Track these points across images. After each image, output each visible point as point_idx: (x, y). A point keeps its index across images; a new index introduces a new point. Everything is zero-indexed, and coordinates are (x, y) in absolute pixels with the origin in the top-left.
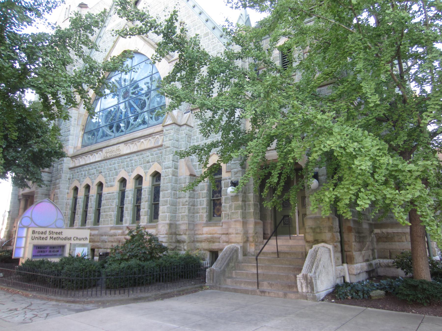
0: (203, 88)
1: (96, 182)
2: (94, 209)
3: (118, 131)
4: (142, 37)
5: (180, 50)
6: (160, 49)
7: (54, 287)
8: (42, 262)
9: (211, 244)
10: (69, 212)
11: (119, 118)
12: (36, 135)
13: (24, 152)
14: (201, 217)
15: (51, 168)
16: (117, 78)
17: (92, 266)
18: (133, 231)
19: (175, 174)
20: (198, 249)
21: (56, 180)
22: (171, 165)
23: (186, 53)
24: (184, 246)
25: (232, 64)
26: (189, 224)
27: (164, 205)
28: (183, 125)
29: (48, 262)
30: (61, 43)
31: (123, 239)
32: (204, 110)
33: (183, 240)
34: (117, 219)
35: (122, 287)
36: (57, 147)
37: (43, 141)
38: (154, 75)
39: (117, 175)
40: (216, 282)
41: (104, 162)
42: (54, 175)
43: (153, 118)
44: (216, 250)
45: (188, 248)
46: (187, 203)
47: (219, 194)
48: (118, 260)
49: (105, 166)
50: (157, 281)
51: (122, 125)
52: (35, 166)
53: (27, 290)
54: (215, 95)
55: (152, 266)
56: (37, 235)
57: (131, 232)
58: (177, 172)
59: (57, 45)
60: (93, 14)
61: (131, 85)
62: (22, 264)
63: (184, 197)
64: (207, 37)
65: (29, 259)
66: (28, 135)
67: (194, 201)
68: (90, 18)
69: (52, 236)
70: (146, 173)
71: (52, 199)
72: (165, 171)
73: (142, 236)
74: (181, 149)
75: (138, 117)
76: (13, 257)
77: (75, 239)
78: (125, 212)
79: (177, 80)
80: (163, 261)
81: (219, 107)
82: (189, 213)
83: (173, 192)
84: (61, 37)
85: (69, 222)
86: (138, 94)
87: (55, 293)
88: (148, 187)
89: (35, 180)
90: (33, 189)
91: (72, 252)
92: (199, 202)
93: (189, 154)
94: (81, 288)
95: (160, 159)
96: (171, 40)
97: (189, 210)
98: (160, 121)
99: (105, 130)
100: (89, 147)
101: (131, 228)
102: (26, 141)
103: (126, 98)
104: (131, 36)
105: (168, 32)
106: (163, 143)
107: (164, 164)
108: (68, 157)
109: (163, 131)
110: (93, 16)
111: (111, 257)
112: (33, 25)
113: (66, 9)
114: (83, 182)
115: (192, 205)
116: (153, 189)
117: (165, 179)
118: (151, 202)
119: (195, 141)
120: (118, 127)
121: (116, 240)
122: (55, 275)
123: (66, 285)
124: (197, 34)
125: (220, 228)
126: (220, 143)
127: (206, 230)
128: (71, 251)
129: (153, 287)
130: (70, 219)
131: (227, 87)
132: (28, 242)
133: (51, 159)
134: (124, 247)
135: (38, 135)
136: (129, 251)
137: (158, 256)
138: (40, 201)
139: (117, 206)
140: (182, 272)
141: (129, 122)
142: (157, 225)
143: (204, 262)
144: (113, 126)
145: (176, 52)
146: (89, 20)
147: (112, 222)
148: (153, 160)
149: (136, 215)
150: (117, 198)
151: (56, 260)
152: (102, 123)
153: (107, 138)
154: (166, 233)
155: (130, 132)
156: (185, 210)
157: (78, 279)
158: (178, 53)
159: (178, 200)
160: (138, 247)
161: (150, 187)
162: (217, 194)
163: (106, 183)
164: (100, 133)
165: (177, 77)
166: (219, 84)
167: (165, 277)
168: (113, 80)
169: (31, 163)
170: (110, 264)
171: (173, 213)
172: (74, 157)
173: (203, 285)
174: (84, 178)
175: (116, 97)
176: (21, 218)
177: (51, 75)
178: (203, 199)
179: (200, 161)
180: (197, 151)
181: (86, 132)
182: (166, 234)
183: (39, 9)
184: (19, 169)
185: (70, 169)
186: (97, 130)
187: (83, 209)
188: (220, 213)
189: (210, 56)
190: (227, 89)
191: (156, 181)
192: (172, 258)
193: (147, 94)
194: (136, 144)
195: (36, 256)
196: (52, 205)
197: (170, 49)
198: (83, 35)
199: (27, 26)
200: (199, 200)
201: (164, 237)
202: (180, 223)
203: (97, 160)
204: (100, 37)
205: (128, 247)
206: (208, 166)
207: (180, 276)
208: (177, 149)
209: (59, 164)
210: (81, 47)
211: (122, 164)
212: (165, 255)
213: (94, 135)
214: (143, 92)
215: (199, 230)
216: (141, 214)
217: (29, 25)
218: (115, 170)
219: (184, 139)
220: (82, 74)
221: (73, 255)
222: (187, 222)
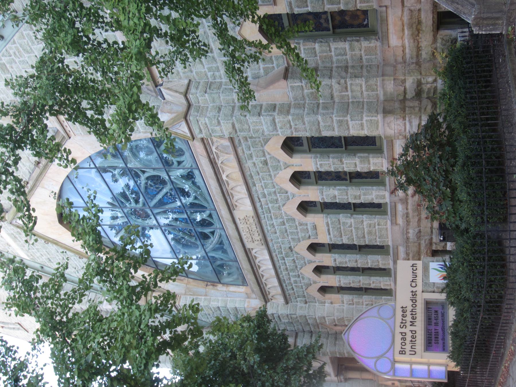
0: (109, 61)
1: (308, 256)
2: (358, 256)
3: (210, 224)
4: (30, 191)
5: (41, 114)
6: (47, 154)
7: (500, 311)
8: (455, 334)
9: (424, 29)
10: (366, 299)
11: (187, 222)
12: (231, 360)
13: (263, 376)
14: (369, 51)
15: (286, 333)
16: (112, 233)
17: (465, 250)
18: (399, 183)
19: (285, 109)
20: (433, 53)
21: (309, 324)
22: (269, 119)
23: (45, 99)
24: (427, 83)
25: (55, 7)
26: (383, 75)
27: (348, 126)
28: (187, 99)
29: (456, 324)
30: (63, 328)
31: (413, 200)
32: (154, 58)
33: (415, 85)
34: (376, 213)
35: (505, 194)
36: (250, 325)
37: (240, 349)
38: (97, 166)
39: (294, 220)
40: (501, 11)
41: (270, 245)
42: (300, 327)
43: (178, 159)
44: (436, 16)
45: (431, 75)
46: (342, 81)
47: (320, 18)
48: (453, 205)
49: (278, 243)
50: (494, 131)
51: (199, 218)
52: (286, 357)
53: (503, 354)
54: (119, 37)
55: (466, 140)
56: (408, 347)
57: (401, 186)
58: (282, 105)
59: (69, 334)
60: (3, 278)
61: (122, 206)
62: (456, 366)
63: (331, 87)
64: (8, 66)
65: (449, 357)
66: (232, 373)
67: (337, 67)
68: (11, 282)
69: (408, 324)
70: (287, 166)
71: (343, 327)
72: (281, 128)
73: (408, 165)
74: (236, 101)
75: (180, 189)
76: (446, 381)
77: (414, 284)
78: (363, 199)
79: (100, 117)
80: (457, 122)
81: (142, 24)
82: (361, 77)
83: (321, 111)
84: (54, 328)
85: (383, 297)
86: (137, 193)
87: (510, 308)
88: (313, 160)
89: (311, 355)
90: (327, 359)
91: (438, 288)
92: (340, 57)
93: (244, 83)
94: (504, 266)
95: (257, 140)
96: (24, 134)
97: (356, 77)
98: (184, 147)
99: (211, 246)
100: (245, 272)
101: (393, 187)
102: (243, 374)
103: (146, 213)
104: (31, 208)
105: (11, 140)
106: (227, 136)
107: (266, 133)
108: (265, 307)
109: (202, 139)
110: (6, 277)
111: (447, 219)
112: (41, 372)
113: (4, 329)
114: (309, 279)
115: (346, 72)
116: (318, 149)
117: (296, 129)
118: (342, 152)
119: (217, 74)
120: (204, 223)
121: (416, 214)
122: (479, 311)
123: (496, 291)
124: (4, 82)
125: (390, 11)
126: (216, 19)
127: (394, 40)
128: (436, 290)
129: (507, 136)
130: (378, 297)
131: (101, 13)
132: (419, 360)
133: (271, 334)
134: (428, 196)
135: (230, 356)
136: (438, 186)
137: (447, 133)
138: (348, 347)
139: (352, 215)
140: (478, 82)
141: (192, 205)
142: (386, 137)
143: (459, 39)
144: (201, 233)
145: (45, 122)
146: (14, 284)
147: (382, 222)
148: (261, 153)
149: (371, 209)
150: (337, 216)
151: (452, 313)
152: (199, 252)
153: (225, 242)
154: (401, 120)
155: (208, 198)
156: (357, 85)
157: (488, 272)
158: (47, 118)
159: (337, 100)
160: (429, 171)
161: (313, 155)
162: (322, 21)
163: (309, 237)
164: (218, 255)
165: (96, 116)
166: (97, 31)
167: (488, 114)
168: (116, 240)
169: (281, 364)
170: (461, 220)
171: (363, 108)
172: (265, 296)
173: (505, 40)
174: (303, 278)
175: (146, 232)
176: (379, 374)
177: (122, 338)
178: (333, 49)
179: (256, 59)
180: (237, 66)
181: (218, 281)
182: (404, 119)
183: (12, 367)
184: (293, 382)
185: (287, 302)
186: (212, 260)
187: (360, 276)
188: (359, 13)
189: (45, 54)
190: (106, 13)
191: (302, 145)
192: (450, 105)
193: (135, 175)
194: (232, 189)
195: (444, 346)
196: (354, 327)
197: (42, 133)
198: (43, 292)
199: (43, 381)
200: (335, 59)
201: (410, 123)
202: (382, 92)
203: (267, 257)
204: (42, 267)
205: (430, 190)
206: (265, 42)
207: (486, 87)
208: (236, 108)
209: (281, 321)
210: (65, 294)
211: (272, 211)
212: (445, 119)
213: (222, 266)
214: (132, 183)
215: (395, 55)
216: (366, 170)
217: (42, 379)
218: (284, 224)
219: (216, 96)
220: (112, 288)
221: (444, 286)
222: (379, 79)
